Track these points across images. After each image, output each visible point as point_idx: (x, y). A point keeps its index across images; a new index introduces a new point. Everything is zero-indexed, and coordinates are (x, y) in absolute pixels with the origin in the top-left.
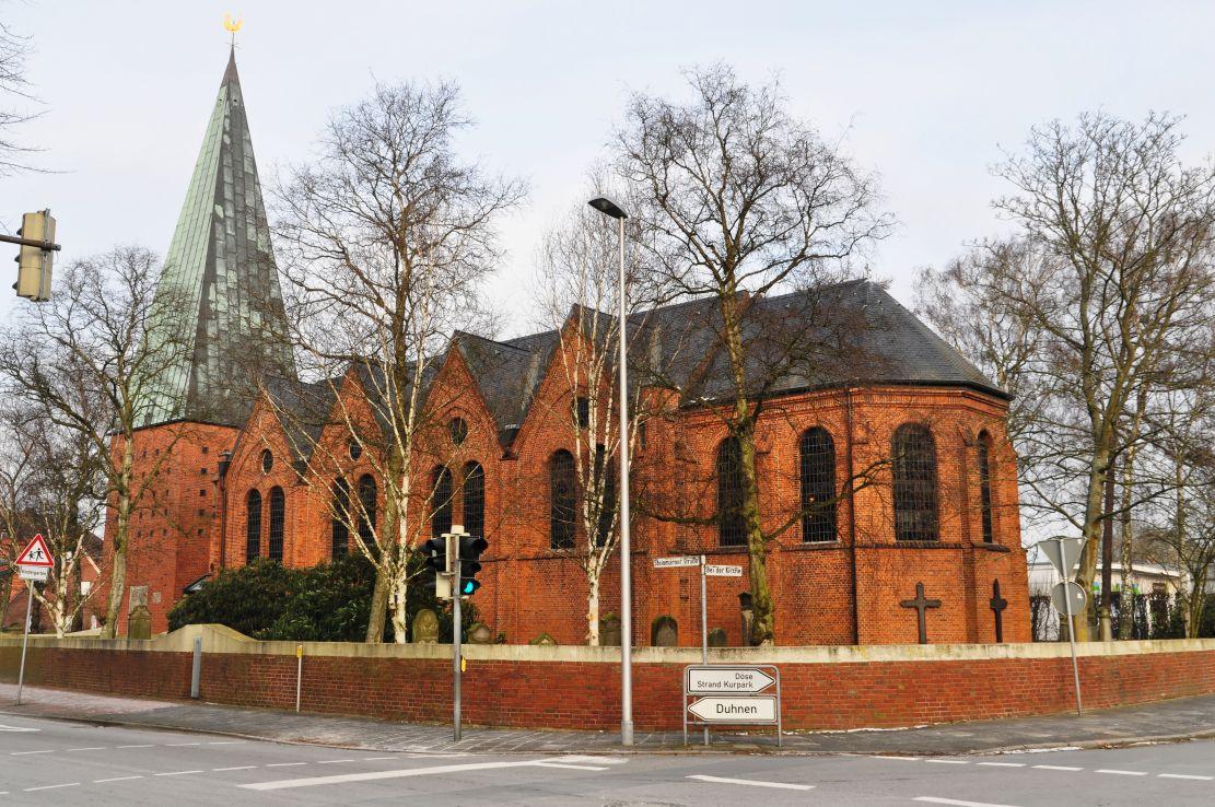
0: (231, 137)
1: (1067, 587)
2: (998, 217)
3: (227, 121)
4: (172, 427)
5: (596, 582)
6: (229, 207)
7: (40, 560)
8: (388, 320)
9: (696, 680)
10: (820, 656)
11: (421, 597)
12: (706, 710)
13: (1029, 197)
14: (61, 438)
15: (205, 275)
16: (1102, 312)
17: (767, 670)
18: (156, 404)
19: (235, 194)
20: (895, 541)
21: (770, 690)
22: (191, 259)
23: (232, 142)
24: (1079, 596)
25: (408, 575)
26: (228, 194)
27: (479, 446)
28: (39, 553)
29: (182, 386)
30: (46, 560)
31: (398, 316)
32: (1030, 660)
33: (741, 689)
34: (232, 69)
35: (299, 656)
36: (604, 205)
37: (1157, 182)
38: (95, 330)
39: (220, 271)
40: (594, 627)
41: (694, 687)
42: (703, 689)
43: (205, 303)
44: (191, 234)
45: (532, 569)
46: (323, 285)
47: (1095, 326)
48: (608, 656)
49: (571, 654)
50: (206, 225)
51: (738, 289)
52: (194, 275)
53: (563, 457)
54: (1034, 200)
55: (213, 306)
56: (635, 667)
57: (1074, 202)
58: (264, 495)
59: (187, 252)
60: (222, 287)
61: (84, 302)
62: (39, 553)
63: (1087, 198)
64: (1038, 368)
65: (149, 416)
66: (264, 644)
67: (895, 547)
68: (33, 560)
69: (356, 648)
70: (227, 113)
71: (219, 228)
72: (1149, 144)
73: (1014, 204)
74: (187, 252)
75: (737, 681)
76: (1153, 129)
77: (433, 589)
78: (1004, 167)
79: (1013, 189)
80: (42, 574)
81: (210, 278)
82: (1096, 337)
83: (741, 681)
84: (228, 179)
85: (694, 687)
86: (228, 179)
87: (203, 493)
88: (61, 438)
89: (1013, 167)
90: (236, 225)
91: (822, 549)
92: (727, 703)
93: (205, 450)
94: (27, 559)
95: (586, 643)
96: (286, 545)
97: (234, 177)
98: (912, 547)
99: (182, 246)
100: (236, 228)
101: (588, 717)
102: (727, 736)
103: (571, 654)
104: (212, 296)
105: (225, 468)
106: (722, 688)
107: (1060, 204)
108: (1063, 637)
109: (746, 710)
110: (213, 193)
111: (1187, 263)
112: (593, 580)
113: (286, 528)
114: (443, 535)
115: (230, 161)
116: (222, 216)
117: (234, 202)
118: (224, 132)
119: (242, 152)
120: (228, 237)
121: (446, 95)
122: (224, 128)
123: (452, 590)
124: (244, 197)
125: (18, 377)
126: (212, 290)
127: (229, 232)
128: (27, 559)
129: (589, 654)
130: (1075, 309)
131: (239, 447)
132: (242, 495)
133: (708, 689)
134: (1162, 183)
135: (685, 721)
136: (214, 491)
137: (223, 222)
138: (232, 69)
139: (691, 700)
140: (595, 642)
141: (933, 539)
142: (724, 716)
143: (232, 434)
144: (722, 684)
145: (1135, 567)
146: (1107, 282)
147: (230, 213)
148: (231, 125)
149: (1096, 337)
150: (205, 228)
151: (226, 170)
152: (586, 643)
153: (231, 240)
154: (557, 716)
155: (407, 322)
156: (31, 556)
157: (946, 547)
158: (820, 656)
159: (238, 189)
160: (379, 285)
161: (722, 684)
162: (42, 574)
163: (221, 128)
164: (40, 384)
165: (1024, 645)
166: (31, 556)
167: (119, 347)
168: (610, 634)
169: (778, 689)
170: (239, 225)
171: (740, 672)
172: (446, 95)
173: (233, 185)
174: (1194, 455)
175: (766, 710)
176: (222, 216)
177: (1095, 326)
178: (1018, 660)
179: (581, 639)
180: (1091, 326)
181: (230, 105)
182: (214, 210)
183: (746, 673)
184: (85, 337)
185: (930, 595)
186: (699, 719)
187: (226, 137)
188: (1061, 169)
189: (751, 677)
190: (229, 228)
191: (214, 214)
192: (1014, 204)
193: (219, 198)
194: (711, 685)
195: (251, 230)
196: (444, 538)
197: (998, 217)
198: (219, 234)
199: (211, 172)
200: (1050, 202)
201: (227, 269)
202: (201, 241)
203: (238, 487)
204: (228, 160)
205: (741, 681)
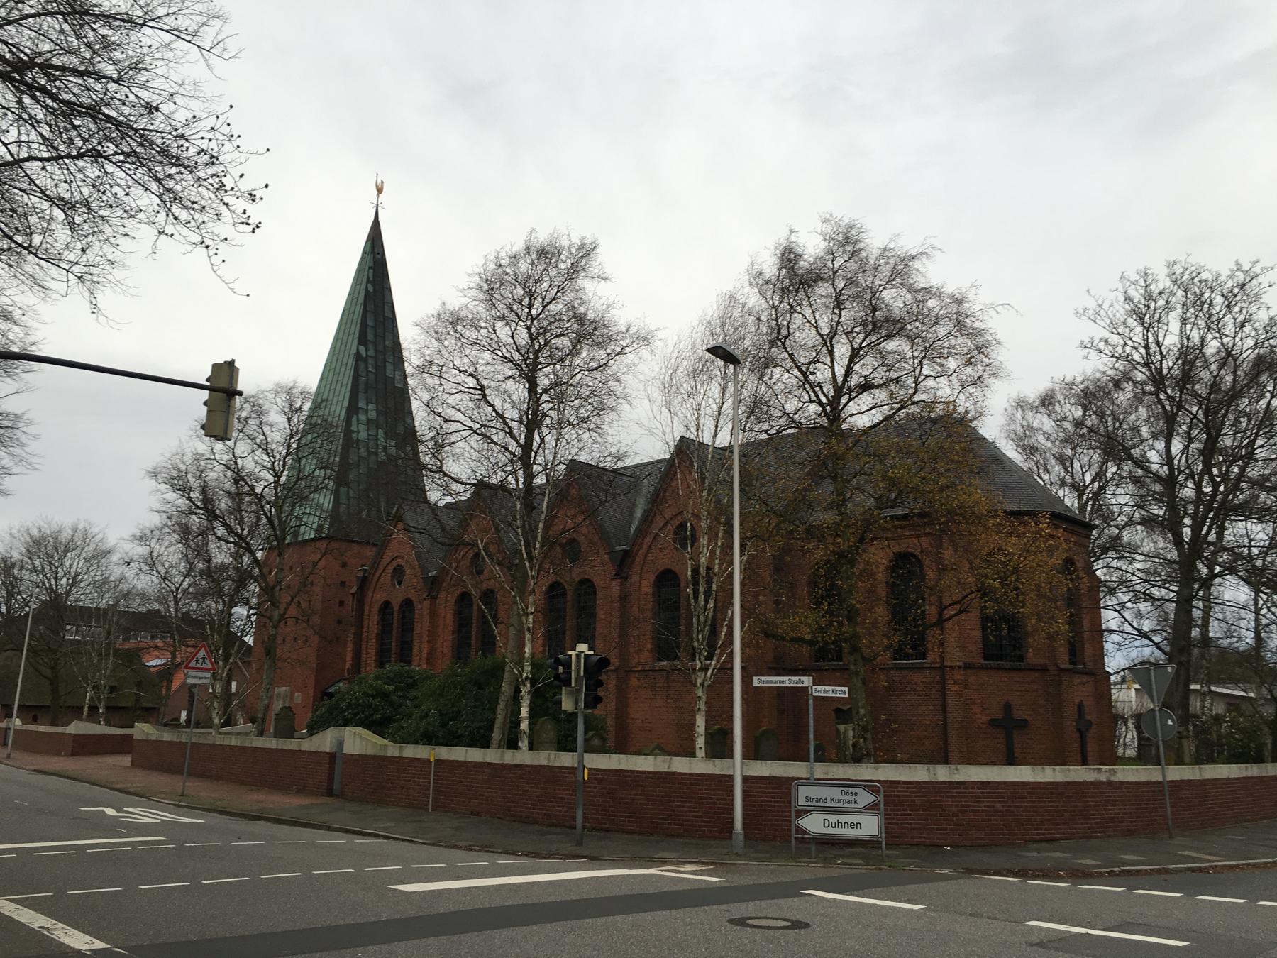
0: (374, 286)
1: (1157, 713)
2: (1086, 357)
3: (371, 271)
4: (318, 544)
5: (704, 697)
6: (371, 346)
7: (204, 666)
8: (518, 452)
9: (804, 795)
10: (919, 773)
11: (544, 706)
12: (813, 824)
13: (1115, 339)
14: (221, 555)
15: (348, 408)
16: (1186, 448)
17: (872, 787)
18: (309, 523)
19: (376, 336)
20: (982, 661)
21: (871, 809)
22: (337, 393)
23: (374, 290)
24: (1170, 722)
25: (531, 687)
26: (370, 336)
27: (598, 569)
28: (204, 659)
29: (326, 504)
30: (209, 666)
31: (527, 448)
32: (1122, 783)
33: (846, 805)
34: (376, 226)
35: (432, 759)
36: (720, 352)
37: (1242, 326)
38: (256, 458)
39: (362, 405)
40: (701, 742)
41: (802, 802)
42: (809, 804)
43: (348, 432)
44: (337, 371)
45: (639, 679)
46: (460, 417)
47: (1179, 461)
48: (714, 767)
49: (680, 765)
50: (350, 361)
51: (844, 426)
52: (333, 407)
53: (667, 579)
54: (1121, 342)
55: (354, 435)
56: (746, 779)
57: (1158, 344)
58: (396, 608)
59: (333, 387)
60: (363, 417)
61: (249, 432)
62: (204, 659)
63: (1171, 340)
64: (1121, 498)
65: (296, 534)
66: (1200, 769)
67: (981, 668)
68: (198, 665)
69: (502, 756)
70: (371, 265)
71: (362, 365)
72: (1236, 290)
73: (1102, 345)
74: (333, 387)
75: (842, 798)
76: (1240, 277)
77: (560, 703)
78: (1091, 312)
79: (1099, 332)
80: (206, 678)
81: (352, 410)
82: (1180, 472)
83: (846, 798)
84: (370, 322)
85: (802, 802)
86: (370, 322)
87: (341, 603)
88: (221, 555)
89: (1102, 313)
90: (376, 363)
91: (913, 668)
92: (833, 818)
93: (344, 565)
94: (193, 664)
95: (693, 755)
96: (415, 652)
97: (376, 321)
98: (999, 669)
99: (329, 382)
100: (376, 367)
101: (700, 826)
102: (830, 846)
103: (680, 765)
104: (354, 428)
105: (364, 582)
106: (829, 804)
107: (1147, 347)
108: (512, 745)
109: (852, 825)
110: (357, 335)
111: (1269, 403)
112: (700, 693)
113: (415, 637)
114: (569, 653)
115: (373, 307)
116: (364, 355)
117: (375, 344)
118: (368, 281)
119: (383, 300)
120: (370, 374)
121: (586, 252)
122: (368, 278)
123: (576, 703)
124: (384, 337)
125: (189, 499)
126: (354, 419)
127: (370, 369)
128: (193, 664)
129: (700, 765)
130: (1160, 445)
131: (375, 563)
132: (376, 608)
133: (814, 804)
134: (1247, 329)
135: (794, 835)
136: (350, 602)
137: (365, 360)
138: (376, 226)
139: (798, 816)
140: (701, 754)
141: (1020, 661)
142: (830, 831)
143: (370, 552)
144: (829, 800)
145: (1213, 689)
146: (1192, 419)
147: (371, 353)
148: (374, 275)
149: (1180, 472)
150: (349, 366)
151: (369, 315)
152: (693, 755)
153: (372, 377)
154: (670, 824)
155: (536, 453)
156: (197, 661)
157: (1033, 669)
158: (919, 773)
159: (379, 331)
160: (511, 420)
161: (829, 800)
162: (206, 678)
163: (365, 277)
164: (208, 504)
165: (959, 766)
166: (197, 661)
167: (276, 473)
168: (719, 745)
169: (882, 806)
170: (379, 364)
171: (846, 789)
172: (586, 252)
173: (375, 328)
174: (1255, 579)
175: (870, 827)
176: (364, 355)
177: (1179, 461)
178: (1110, 783)
179: (485, 743)
180: (1176, 462)
181: (374, 257)
182: (358, 349)
183: (851, 790)
184: (248, 465)
185: (1017, 714)
186: (805, 833)
187: (369, 285)
188: (1147, 315)
189: (856, 794)
190: (370, 366)
191: (358, 354)
192: (1102, 345)
193: (363, 340)
194: (817, 801)
195: (389, 368)
196: (571, 655)
197: (1086, 357)
198: (362, 372)
199: (355, 317)
200: (1136, 345)
201: (368, 403)
202: (346, 379)
203: (377, 597)
204: (370, 307)
205: (846, 798)
